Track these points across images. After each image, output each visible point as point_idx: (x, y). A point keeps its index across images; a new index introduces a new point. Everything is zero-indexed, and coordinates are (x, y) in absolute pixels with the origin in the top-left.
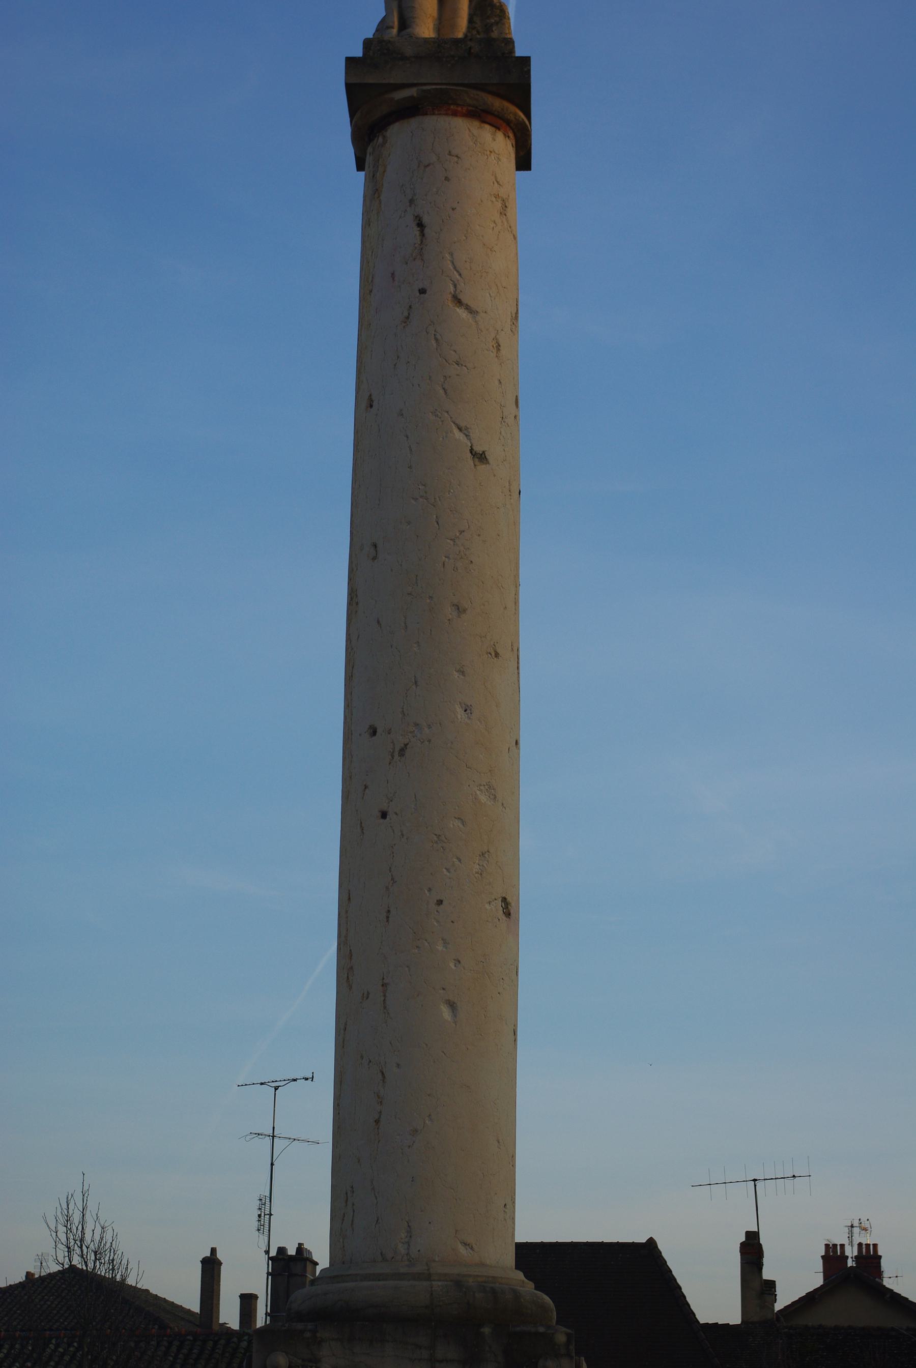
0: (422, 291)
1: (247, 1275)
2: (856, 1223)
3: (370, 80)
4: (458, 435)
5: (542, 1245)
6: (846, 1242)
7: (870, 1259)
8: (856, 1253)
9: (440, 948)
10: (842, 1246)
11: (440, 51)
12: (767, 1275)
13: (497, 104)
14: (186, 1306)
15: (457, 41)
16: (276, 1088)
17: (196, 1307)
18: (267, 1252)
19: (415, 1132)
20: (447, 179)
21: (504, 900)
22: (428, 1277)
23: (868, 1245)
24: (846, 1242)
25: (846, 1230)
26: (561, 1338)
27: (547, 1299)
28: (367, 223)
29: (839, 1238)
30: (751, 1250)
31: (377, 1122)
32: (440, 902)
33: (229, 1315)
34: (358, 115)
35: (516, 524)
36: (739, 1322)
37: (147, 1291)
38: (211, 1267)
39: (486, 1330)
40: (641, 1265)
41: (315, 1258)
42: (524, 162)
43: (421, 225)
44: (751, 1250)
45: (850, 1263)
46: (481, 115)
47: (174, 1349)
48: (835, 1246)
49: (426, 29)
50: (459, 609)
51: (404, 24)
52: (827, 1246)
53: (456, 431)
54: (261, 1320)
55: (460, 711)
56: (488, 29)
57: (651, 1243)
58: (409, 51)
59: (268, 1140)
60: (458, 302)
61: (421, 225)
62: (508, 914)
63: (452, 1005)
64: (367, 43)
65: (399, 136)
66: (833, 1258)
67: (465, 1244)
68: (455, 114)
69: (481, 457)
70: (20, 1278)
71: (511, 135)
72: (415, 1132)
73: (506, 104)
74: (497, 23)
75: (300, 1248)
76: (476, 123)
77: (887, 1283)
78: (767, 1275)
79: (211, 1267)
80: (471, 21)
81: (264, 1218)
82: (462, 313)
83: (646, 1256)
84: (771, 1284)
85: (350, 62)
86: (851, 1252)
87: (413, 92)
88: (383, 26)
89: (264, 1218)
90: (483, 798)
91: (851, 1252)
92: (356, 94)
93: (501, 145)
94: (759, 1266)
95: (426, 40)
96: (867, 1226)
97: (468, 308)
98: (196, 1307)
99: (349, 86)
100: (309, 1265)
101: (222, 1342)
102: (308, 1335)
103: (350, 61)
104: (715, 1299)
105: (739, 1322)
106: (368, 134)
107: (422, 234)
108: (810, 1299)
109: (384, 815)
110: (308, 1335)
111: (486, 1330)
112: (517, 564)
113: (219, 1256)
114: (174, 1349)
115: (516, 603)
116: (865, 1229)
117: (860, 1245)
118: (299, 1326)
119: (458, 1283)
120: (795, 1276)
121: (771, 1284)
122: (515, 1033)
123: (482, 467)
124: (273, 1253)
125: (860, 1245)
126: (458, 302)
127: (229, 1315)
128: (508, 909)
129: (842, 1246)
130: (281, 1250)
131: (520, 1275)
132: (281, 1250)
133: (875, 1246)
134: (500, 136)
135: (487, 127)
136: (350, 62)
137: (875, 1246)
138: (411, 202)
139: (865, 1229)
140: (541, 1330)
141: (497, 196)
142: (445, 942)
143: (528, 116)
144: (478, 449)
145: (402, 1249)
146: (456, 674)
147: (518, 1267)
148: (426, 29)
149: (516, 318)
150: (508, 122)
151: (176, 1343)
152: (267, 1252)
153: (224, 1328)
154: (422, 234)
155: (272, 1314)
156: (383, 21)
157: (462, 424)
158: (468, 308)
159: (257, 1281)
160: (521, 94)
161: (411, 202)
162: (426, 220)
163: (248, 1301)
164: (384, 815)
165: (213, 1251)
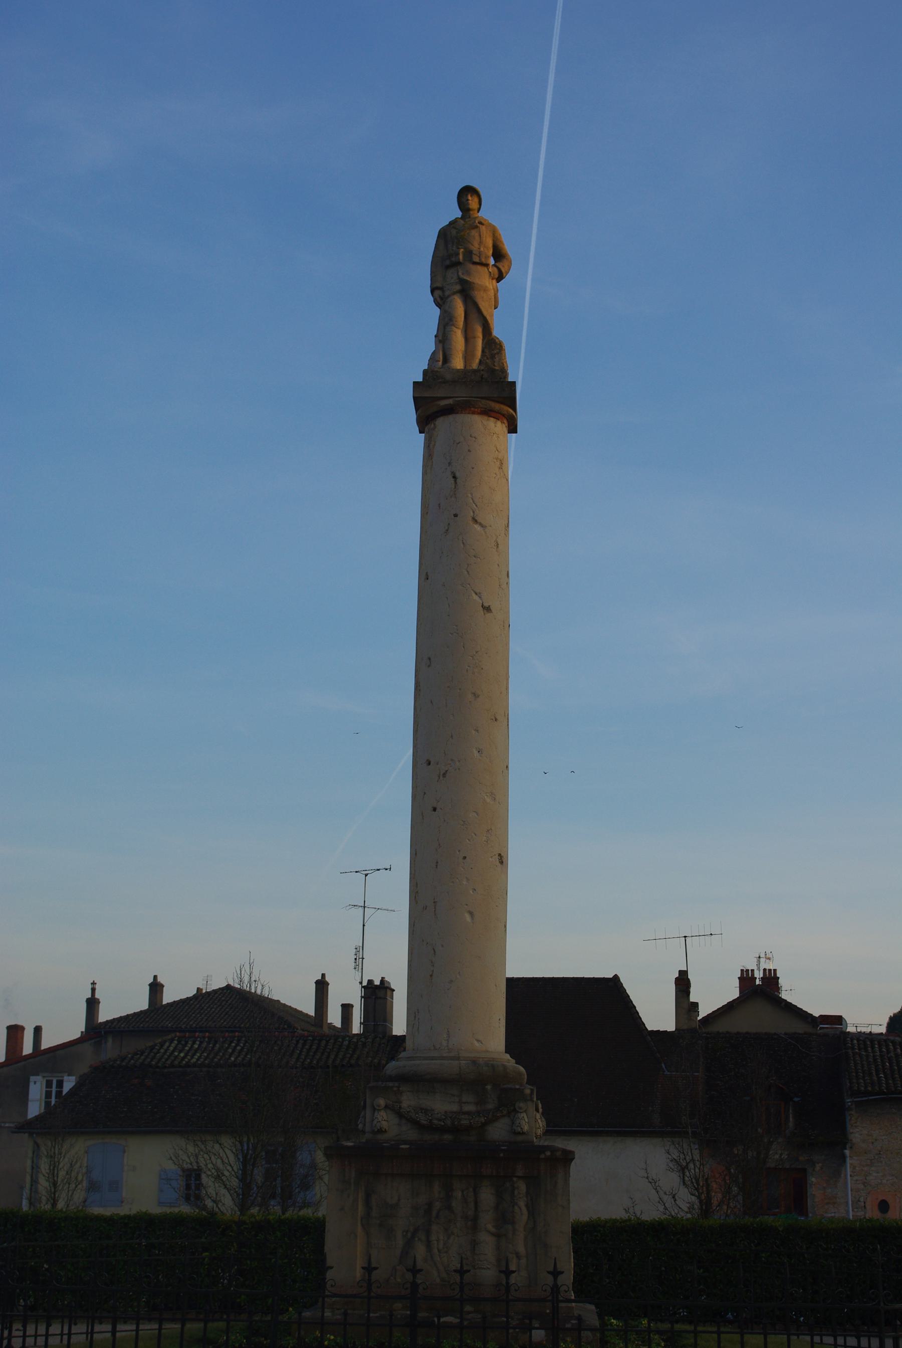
0: (456, 515)
1: (346, 991)
2: (762, 955)
3: (426, 395)
4: (475, 597)
5: (543, 978)
6: (755, 968)
7: (771, 979)
8: (762, 976)
9: (465, 883)
10: (753, 971)
11: (465, 377)
12: (693, 998)
13: (497, 406)
14: (305, 1011)
15: (475, 371)
16: (366, 875)
17: (312, 1012)
18: (361, 983)
19: (452, 981)
20: (469, 451)
21: (500, 855)
22: (458, 1058)
23: (770, 970)
24: (755, 968)
25: (756, 960)
26: (528, 1091)
27: (522, 1069)
28: (425, 473)
29: (751, 965)
30: (683, 983)
31: (431, 976)
32: (465, 858)
33: (334, 1018)
34: (420, 411)
35: (507, 644)
36: (674, 1029)
37: (278, 1001)
38: (322, 986)
39: (489, 1087)
40: (608, 995)
41: (393, 987)
42: (513, 429)
43: (454, 477)
44: (683, 983)
45: (758, 982)
46: (487, 413)
47: (300, 1045)
48: (747, 970)
49: (458, 363)
50: (476, 696)
51: (446, 360)
52: (742, 970)
53: (474, 595)
54: (356, 1028)
55: (475, 752)
56: (493, 357)
57: (616, 977)
58: (448, 377)
59: (361, 910)
60: (475, 521)
61: (454, 477)
62: (502, 863)
63: (471, 914)
64: (425, 373)
65: (442, 423)
66: (746, 979)
67: (478, 1041)
68: (474, 413)
69: (488, 609)
70: (192, 993)
71: (505, 421)
72: (452, 981)
73: (503, 406)
74: (498, 353)
75: (383, 980)
76: (486, 418)
77: (784, 995)
78: (693, 998)
79: (322, 986)
80: (483, 351)
81: (359, 960)
82: (477, 527)
83: (613, 986)
84: (696, 1005)
85: (416, 384)
86: (758, 975)
87: (450, 401)
88: (433, 358)
89: (359, 960)
90: (488, 800)
91: (758, 975)
92: (418, 402)
93: (500, 427)
94: (688, 993)
95: (458, 370)
96: (770, 956)
97: (481, 524)
98: (312, 1012)
99: (414, 398)
100: (389, 992)
101: (332, 1041)
102: (395, 1089)
103: (415, 383)
104: (657, 1013)
105: (674, 1029)
106: (425, 421)
107: (455, 481)
108: (730, 1007)
109: (435, 809)
110: (395, 1089)
111: (489, 1087)
112: (508, 667)
113: (327, 979)
114: (300, 1045)
115: (507, 688)
116: (769, 959)
117: (765, 970)
118: (391, 1084)
119: (474, 1062)
120: (714, 993)
121: (696, 1005)
122: (505, 926)
123: (488, 615)
124: (365, 984)
125: (765, 970)
126: (475, 521)
127: (334, 1018)
128: (502, 860)
129: (753, 971)
130: (370, 982)
131: (508, 1056)
132: (370, 982)
133: (775, 970)
134: (499, 423)
135: (492, 419)
136: (416, 384)
137: (775, 970)
138: (450, 464)
139: (769, 959)
140: (517, 1087)
141: (497, 459)
142: (468, 879)
143: (515, 411)
144: (486, 605)
145: (444, 1043)
146: (474, 732)
147: (507, 1051)
148: (458, 363)
149: (508, 526)
150: (503, 415)
151: (301, 1042)
152: (361, 983)
153: (331, 1026)
154: (455, 481)
155: (365, 1023)
156: (434, 353)
157: (478, 591)
158: (481, 524)
159: (355, 998)
160: (511, 402)
161: (450, 464)
162: (458, 474)
163: (347, 1009)
164: (435, 809)
165: (323, 975)
